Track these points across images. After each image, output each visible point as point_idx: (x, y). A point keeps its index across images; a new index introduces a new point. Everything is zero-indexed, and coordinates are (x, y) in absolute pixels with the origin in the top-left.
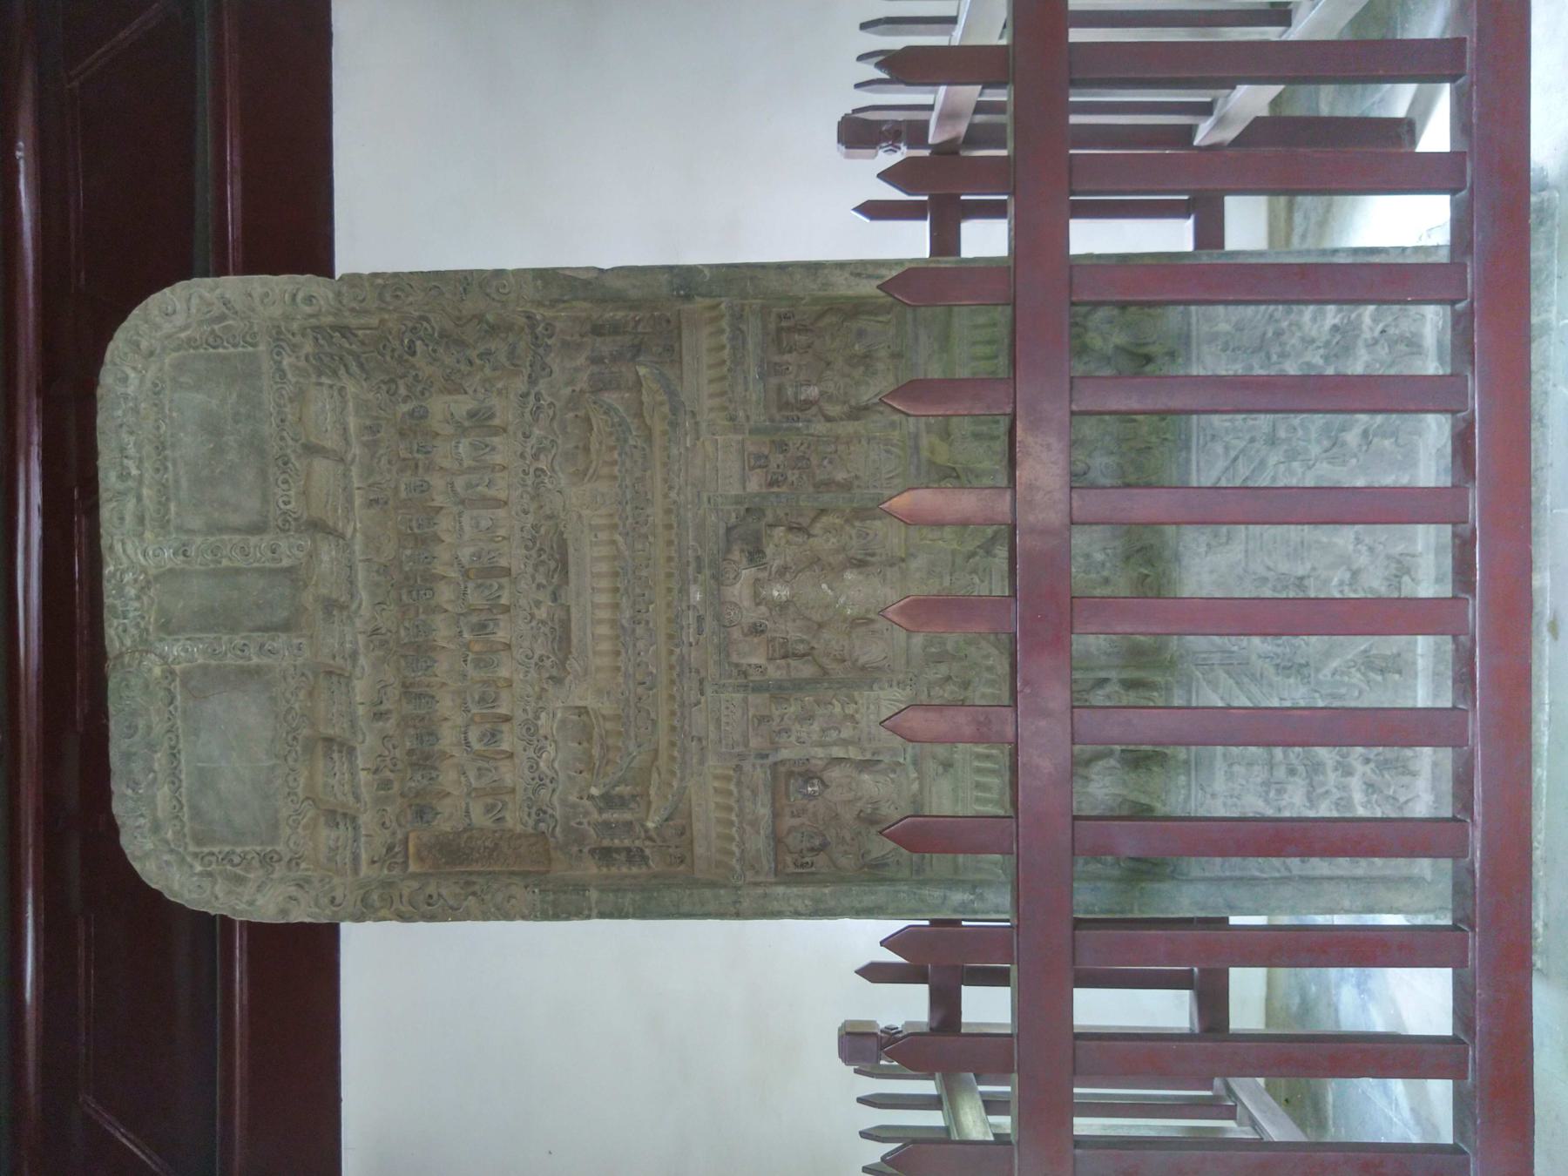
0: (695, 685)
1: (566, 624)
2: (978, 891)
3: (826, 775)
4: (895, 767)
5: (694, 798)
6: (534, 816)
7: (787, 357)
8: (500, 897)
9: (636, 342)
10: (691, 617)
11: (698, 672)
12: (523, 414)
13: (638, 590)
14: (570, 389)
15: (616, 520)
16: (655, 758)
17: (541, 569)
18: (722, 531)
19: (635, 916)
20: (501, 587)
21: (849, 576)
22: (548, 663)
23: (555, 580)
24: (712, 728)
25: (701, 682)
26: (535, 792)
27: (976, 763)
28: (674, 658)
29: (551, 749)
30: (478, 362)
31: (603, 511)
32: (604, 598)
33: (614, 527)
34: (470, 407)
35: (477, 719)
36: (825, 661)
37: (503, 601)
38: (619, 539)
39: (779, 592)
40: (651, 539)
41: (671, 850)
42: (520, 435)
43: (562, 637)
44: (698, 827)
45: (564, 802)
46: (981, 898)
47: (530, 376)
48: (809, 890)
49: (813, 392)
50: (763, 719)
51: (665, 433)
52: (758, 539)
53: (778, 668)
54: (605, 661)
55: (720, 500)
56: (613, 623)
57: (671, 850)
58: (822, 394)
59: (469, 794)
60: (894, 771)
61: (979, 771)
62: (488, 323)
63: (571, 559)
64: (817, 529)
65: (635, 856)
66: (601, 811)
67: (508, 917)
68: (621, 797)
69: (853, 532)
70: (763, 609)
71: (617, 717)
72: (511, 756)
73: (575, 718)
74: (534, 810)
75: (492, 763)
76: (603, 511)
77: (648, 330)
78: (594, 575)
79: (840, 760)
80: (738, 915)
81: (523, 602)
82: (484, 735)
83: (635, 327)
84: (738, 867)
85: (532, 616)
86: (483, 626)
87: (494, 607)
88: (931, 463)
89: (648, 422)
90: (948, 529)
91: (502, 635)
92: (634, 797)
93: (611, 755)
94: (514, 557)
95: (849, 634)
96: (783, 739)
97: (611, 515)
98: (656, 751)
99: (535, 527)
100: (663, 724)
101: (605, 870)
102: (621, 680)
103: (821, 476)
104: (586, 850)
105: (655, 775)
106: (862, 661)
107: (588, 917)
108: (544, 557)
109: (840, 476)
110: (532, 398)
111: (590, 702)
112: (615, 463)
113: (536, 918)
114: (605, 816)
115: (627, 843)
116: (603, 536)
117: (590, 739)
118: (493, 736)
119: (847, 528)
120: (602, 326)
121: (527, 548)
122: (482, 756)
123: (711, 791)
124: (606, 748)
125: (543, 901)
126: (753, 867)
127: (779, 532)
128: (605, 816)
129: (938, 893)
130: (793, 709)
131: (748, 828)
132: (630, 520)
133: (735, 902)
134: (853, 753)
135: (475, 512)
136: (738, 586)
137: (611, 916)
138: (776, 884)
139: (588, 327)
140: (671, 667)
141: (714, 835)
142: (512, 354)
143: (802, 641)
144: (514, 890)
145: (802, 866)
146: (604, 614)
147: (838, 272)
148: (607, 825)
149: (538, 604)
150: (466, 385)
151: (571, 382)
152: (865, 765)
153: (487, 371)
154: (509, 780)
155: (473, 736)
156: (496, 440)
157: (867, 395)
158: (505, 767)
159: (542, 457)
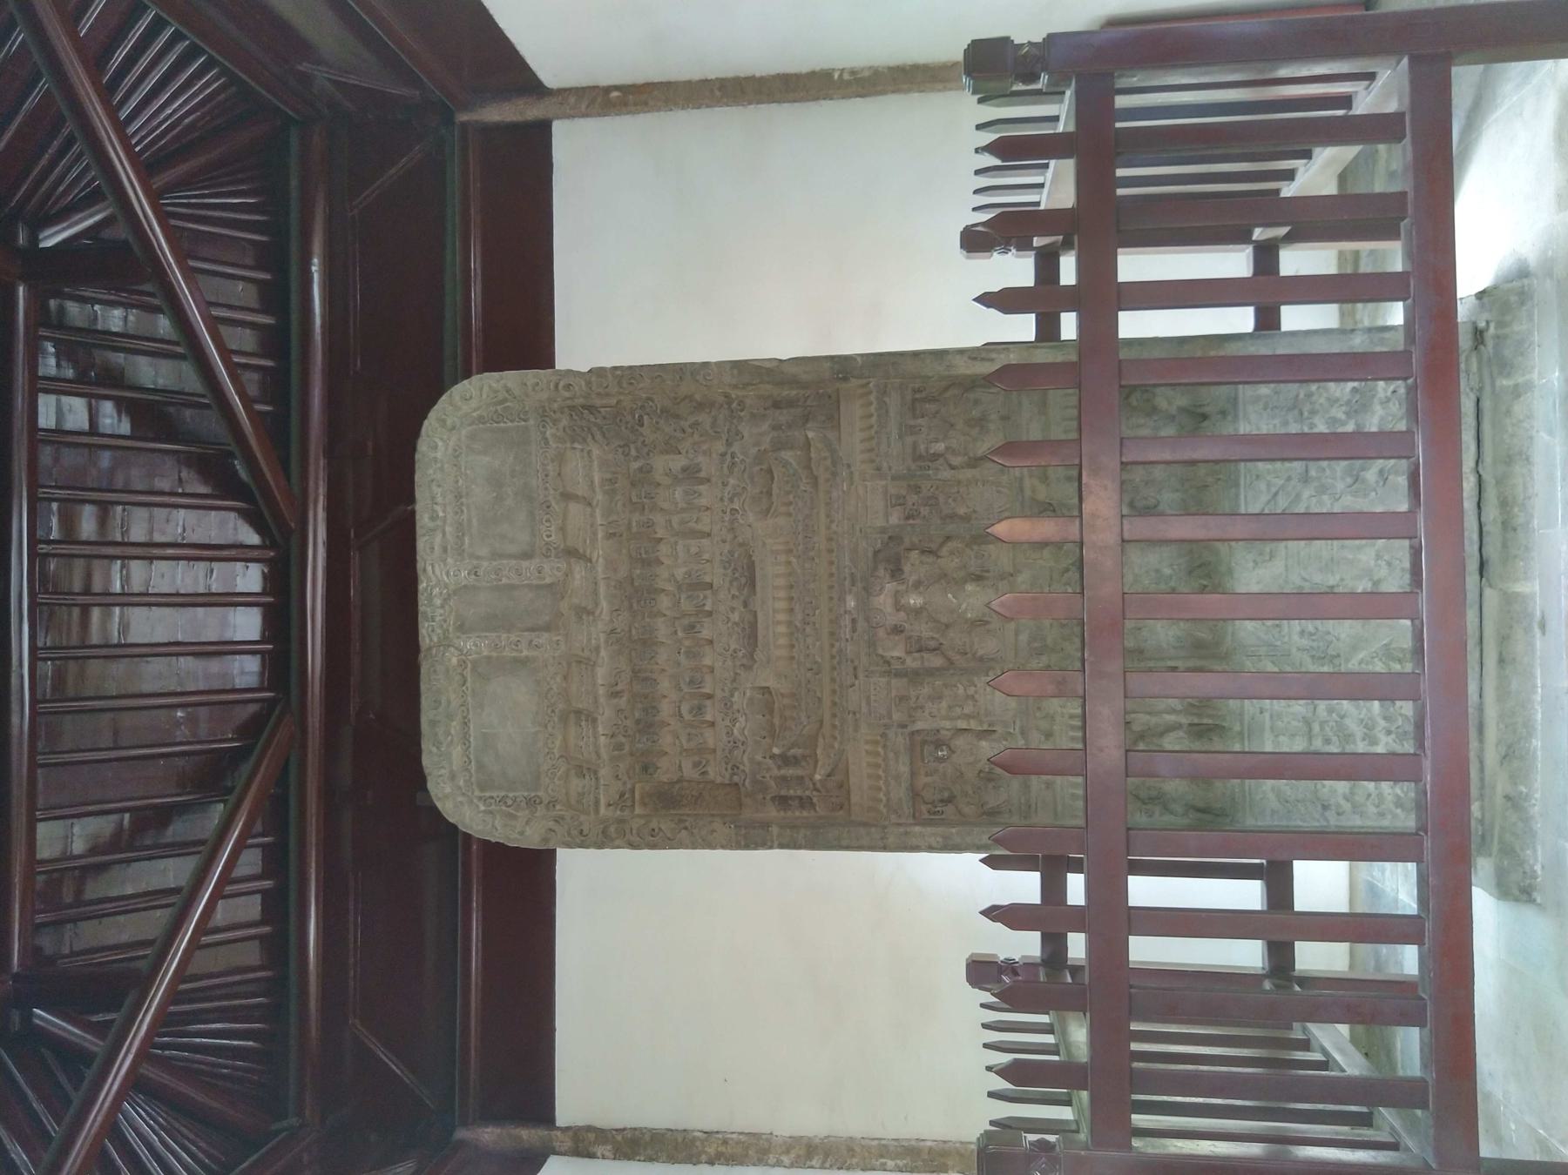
1: (754, 626)
7: (920, 421)
10: (847, 621)
18: (870, 554)
21: (969, 587)
24: (863, 704)
29: (742, 719)
33: (791, 551)
36: (950, 653)
37: (707, 608)
39: (914, 600)
43: (751, 635)
45: (752, 760)
50: (903, 699)
51: (827, 480)
58: (947, 448)
64: (944, 551)
66: (779, 768)
68: (795, 757)
71: (793, 695)
87: (701, 611)
91: (706, 633)
92: (804, 757)
94: (716, 575)
98: (821, 722)
99: (731, 553)
105: (821, 740)
106: (980, 652)
107: (771, 847)
109: (962, 511)
111: (771, 683)
114: (783, 772)
115: (799, 793)
118: (699, 710)
119: (968, 551)
127: (914, 554)
128: (783, 772)
130: (926, 691)
140: (833, 657)
142: (714, 424)
146: (781, 617)
148: (784, 779)
149: (733, 609)
151: (757, 444)
153: (696, 437)
154: (711, 743)
155: (685, 708)
156: (702, 488)
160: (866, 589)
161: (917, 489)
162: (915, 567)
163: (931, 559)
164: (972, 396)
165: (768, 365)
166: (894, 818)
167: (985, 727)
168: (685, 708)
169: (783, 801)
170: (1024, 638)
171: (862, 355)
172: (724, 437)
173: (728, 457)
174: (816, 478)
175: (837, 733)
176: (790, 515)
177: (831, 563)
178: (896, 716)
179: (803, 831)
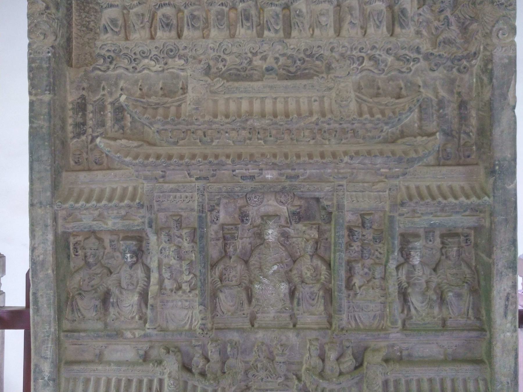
0: (204, 174)
1: (249, 78)
2: (51, 383)
3: (139, 266)
4: (143, 318)
5: (122, 171)
6: (108, 54)
7: (438, 240)
8: (45, 27)
9: (454, 133)
10: (253, 171)
11: (214, 175)
12: (403, 48)
13: (274, 132)
14: (421, 84)
15: (329, 116)
16: (150, 144)
17: (289, 61)
18: (317, 194)
19: (31, 128)
20: (277, 31)
21: (284, 287)
22: (220, 65)
23: (281, 71)
24: (172, 186)
25: (206, 178)
26: (126, 55)
27: (145, 380)
28: (224, 159)
29: (157, 68)
30: (442, 17)
31: (335, 106)
32: (269, 107)
33: (324, 115)
34: (409, 10)
35: (180, 14)
36: (221, 267)
37: (266, 33)
38: (314, 119)
39: (272, 234)
40: (312, 142)
41: (85, 155)
42: (389, 46)
43: (240, 75)
44: (99, 175)
45: (119, 77)
46: (46, 385)
47: (432, 54)
48: (50, 259)
49: (416, 260)
50: (179, 223)
51: (393, 153)
52: (308, 218)
53: (216, 232)
54: (221, 107)
55: (341, 193)
56: (250, 114)
57: (85, 155)
58: (413, 266)
59: (125, 8)
60: (140, 318)
61: (140, 382)
62: (470, 24)
63: (298, 82)
64: (318, 263)
65: (80, 128)
66: (112, 103)
67: (30, 32)
68: (123, 118)
69: (315, 289)
70: (259, 221)
71: (178, 115)
72: (152, 38)
73: (180, 86)
74: (112, 54)
75: (148, 25)
76: (335, 106)
77: (462, 142)
78: (286, 99)
79: (149, 278)
80: (32, 205)
81: (266, 47)
82: (168, 18)
83: (465, 133)
84: (67, 205)
85: (255, 54)
86: (248, 18)
87: (261, 27)
88: (366, 349)
89: (399, 141)
90: (319, 362)
91: (241, 31)
92: (122, 128)
93: (150, 111)
94: (299, 41)
95: (239, 285)
96: (164, 238)
97: (332, 112)
98: (154, 145)
99: (320, 57)
100: (175, 150)
101: (70, 106)
102: (207, 118)
103: (358, 267)
104: (84, 93)
105: (135, 144)
106: (221, 296)
107: (30, 93)
108: (298, 63)
109: (357, 281)
110: (415, 55)
111: (191, 95)
112: (372, 115)
113: (30, 54)
114: (109, 107)
115: (90, 123)
116: (316, 106)
117: (164, 95)
118: (167, 25)
119: (318, 286)
120: (466, 108)
121: (306, 50)
122: (153, 18)
123: (125, 185)
124: (156, 107)
125: (42, 59)
126: (70, 215)
127: (315, 234)
128: (109, 107)
129: (49, 353)
130: (186, 245)
131: (96, 213)
132: (327, 126)
133: (41, 203)
134: (153, 288)
135: (331, 13)
136: (275, 203)
137: (31, 110)
138: (56, 235)
139: (466, 98)
140: (216, 157)
141: (93, 187)
142: (448, 42)
143: (235, 250)
144: (51, 39)
145: (75, 248)
146: (257, 106)
147: (510, 284)
148: (103, 108)
149: (264, 58)
150: (425, 8)
151: (426, 85)
152: (144, 295)
153: (436, 23)
154: (135, 36)
155: (168, 11)
156: (384, 29)
157: (415, 300)
158: (145, 33)
159: (372, 63)
160: (283, 191)
161: (378, 239)
162: (303, 234)
163: (310, 249)
164: (465, 291)
165: (510, 95)
166: (62, 214)
167: (150, 301)
168: (168, 11)
169: (81, 107)
170: (235, 336)
171: (515, 190)
172: (435, 51)
173: (414, 55)
174: (393, 142)
175: (140, 160)
176: (361, 114)
177: (310, 156)
178: (162, 216)
179: (46, 124)
